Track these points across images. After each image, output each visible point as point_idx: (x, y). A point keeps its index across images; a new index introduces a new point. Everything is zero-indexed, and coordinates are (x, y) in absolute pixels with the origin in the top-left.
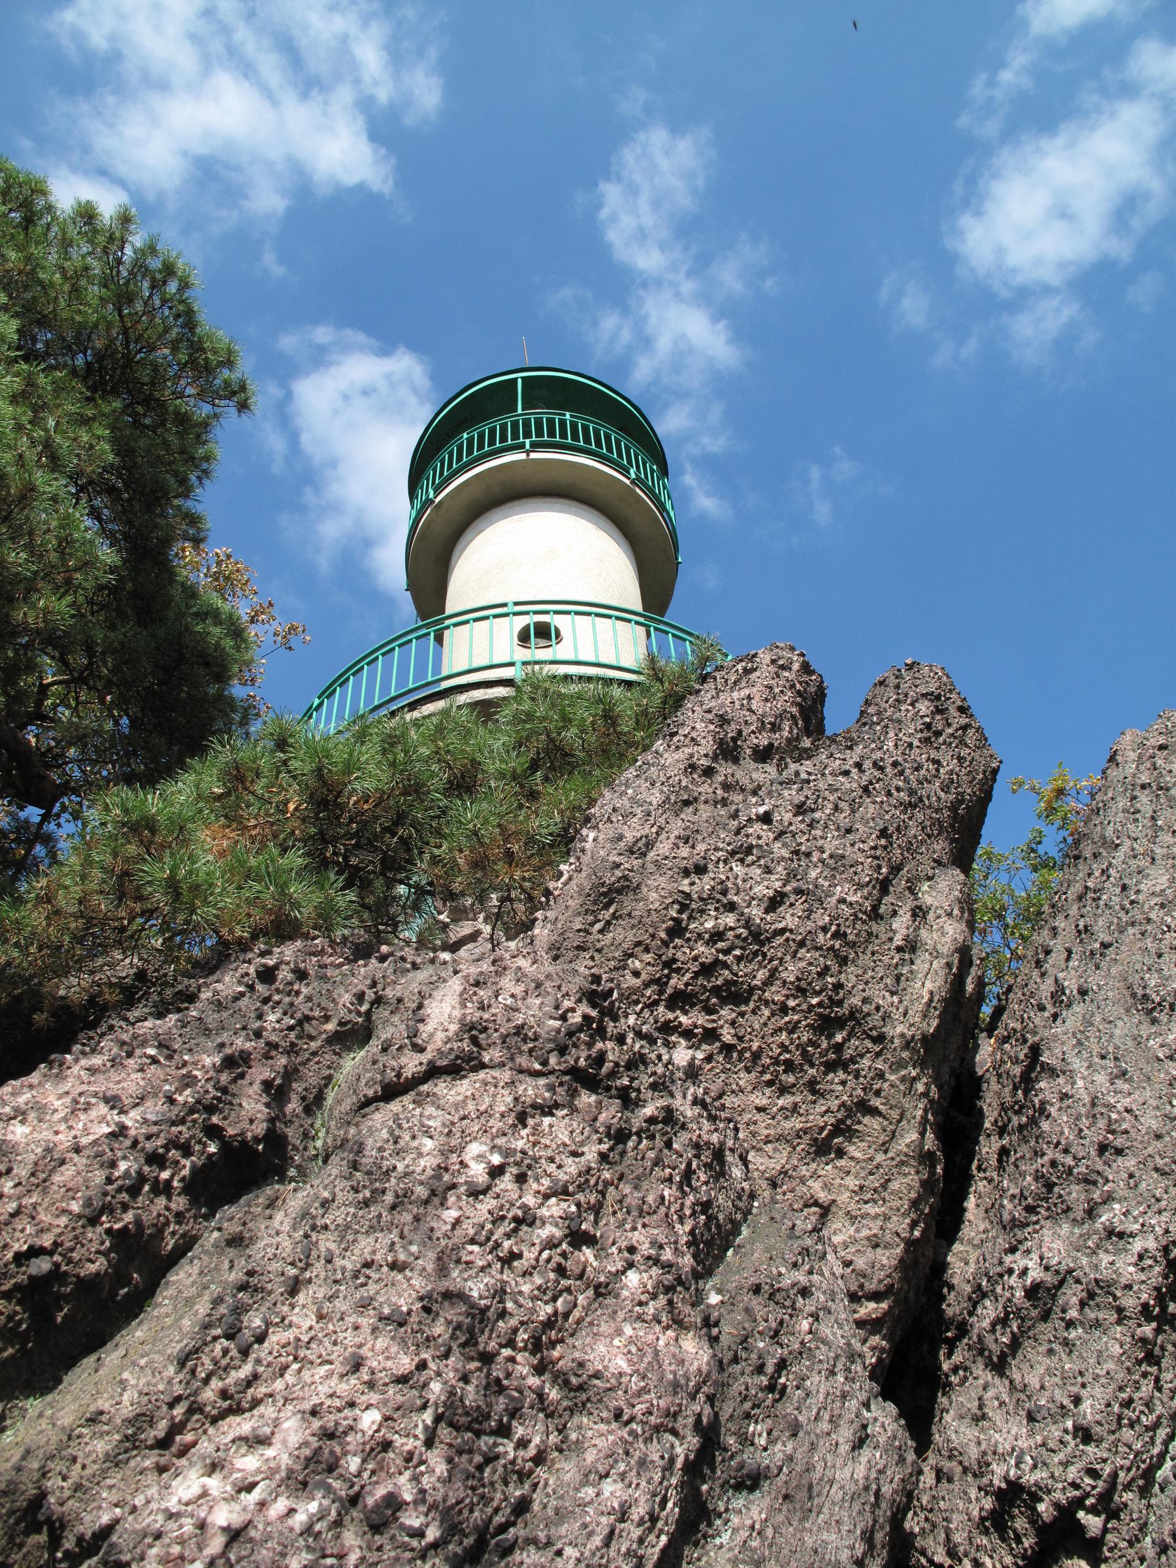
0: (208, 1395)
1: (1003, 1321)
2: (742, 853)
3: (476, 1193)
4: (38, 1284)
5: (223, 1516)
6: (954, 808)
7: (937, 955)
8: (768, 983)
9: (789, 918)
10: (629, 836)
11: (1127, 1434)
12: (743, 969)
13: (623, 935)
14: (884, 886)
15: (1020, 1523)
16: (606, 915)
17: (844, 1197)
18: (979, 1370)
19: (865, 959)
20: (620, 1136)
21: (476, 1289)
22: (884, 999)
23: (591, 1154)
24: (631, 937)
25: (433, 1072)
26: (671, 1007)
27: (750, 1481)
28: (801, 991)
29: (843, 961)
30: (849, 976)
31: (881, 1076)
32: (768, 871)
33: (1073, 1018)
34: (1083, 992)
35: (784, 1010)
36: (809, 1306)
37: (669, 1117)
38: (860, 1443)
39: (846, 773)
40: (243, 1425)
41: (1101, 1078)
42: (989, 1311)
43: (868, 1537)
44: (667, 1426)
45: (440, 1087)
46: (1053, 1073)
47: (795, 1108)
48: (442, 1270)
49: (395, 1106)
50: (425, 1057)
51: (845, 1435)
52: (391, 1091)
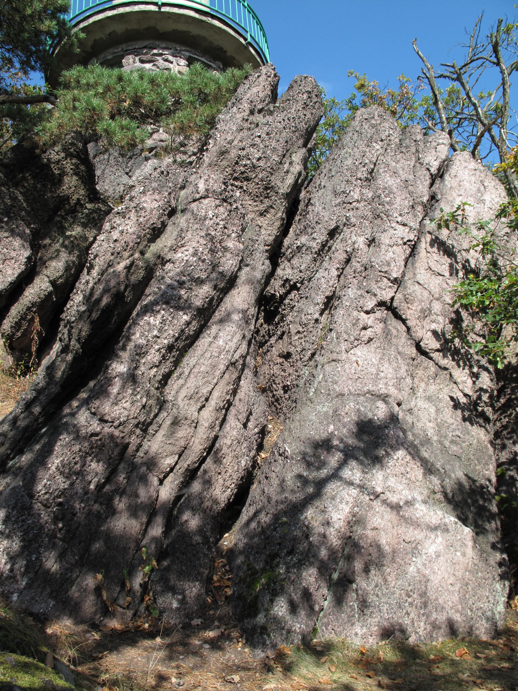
0: (179, 244)
1: (291, 253)
2: (253, 145)
3: (211, 219)
4: (154, 228)
5: (185, 258)
6: (307, 129)
7: (293, 174)
8: (255, 177)
9: (262, 163)
10: (229, 139)
11: (308, 272)
12: (250, 174)
13: (225, 163)
14: (284, 156)
15: (287, 285)
16: (222, 158)
17: (264, 225)
18: (286, 262)
19: (277, 174)
20: (230, 211)
21: (213, 233)
22: (279, 184)
23: (226, 214)
24: (227, 163)
25: (201, 198)
26: (233, 180)
27: (247, 265)
28: (262, 181)
29: (272, 174)
30: (272, 178)
31: (276, 201)
32: (258, 151)
33: (321, 192)
34: (324, 187)
35: (258, 184)
36: (257, 243)
37: (237, 208)
38: (263, 264)
39: (280, 122)
40: (185, 248)
41: (320, 208)
42: (290, 250)
43: (263, 276)
44: (238, 255)
45: (203, 200)
46: (312, 205)
47: (257, 206)
48: (207, 231)
49: (195, 203)
50: (200, 195)
51: (261, 263)
52: (195, 201)
